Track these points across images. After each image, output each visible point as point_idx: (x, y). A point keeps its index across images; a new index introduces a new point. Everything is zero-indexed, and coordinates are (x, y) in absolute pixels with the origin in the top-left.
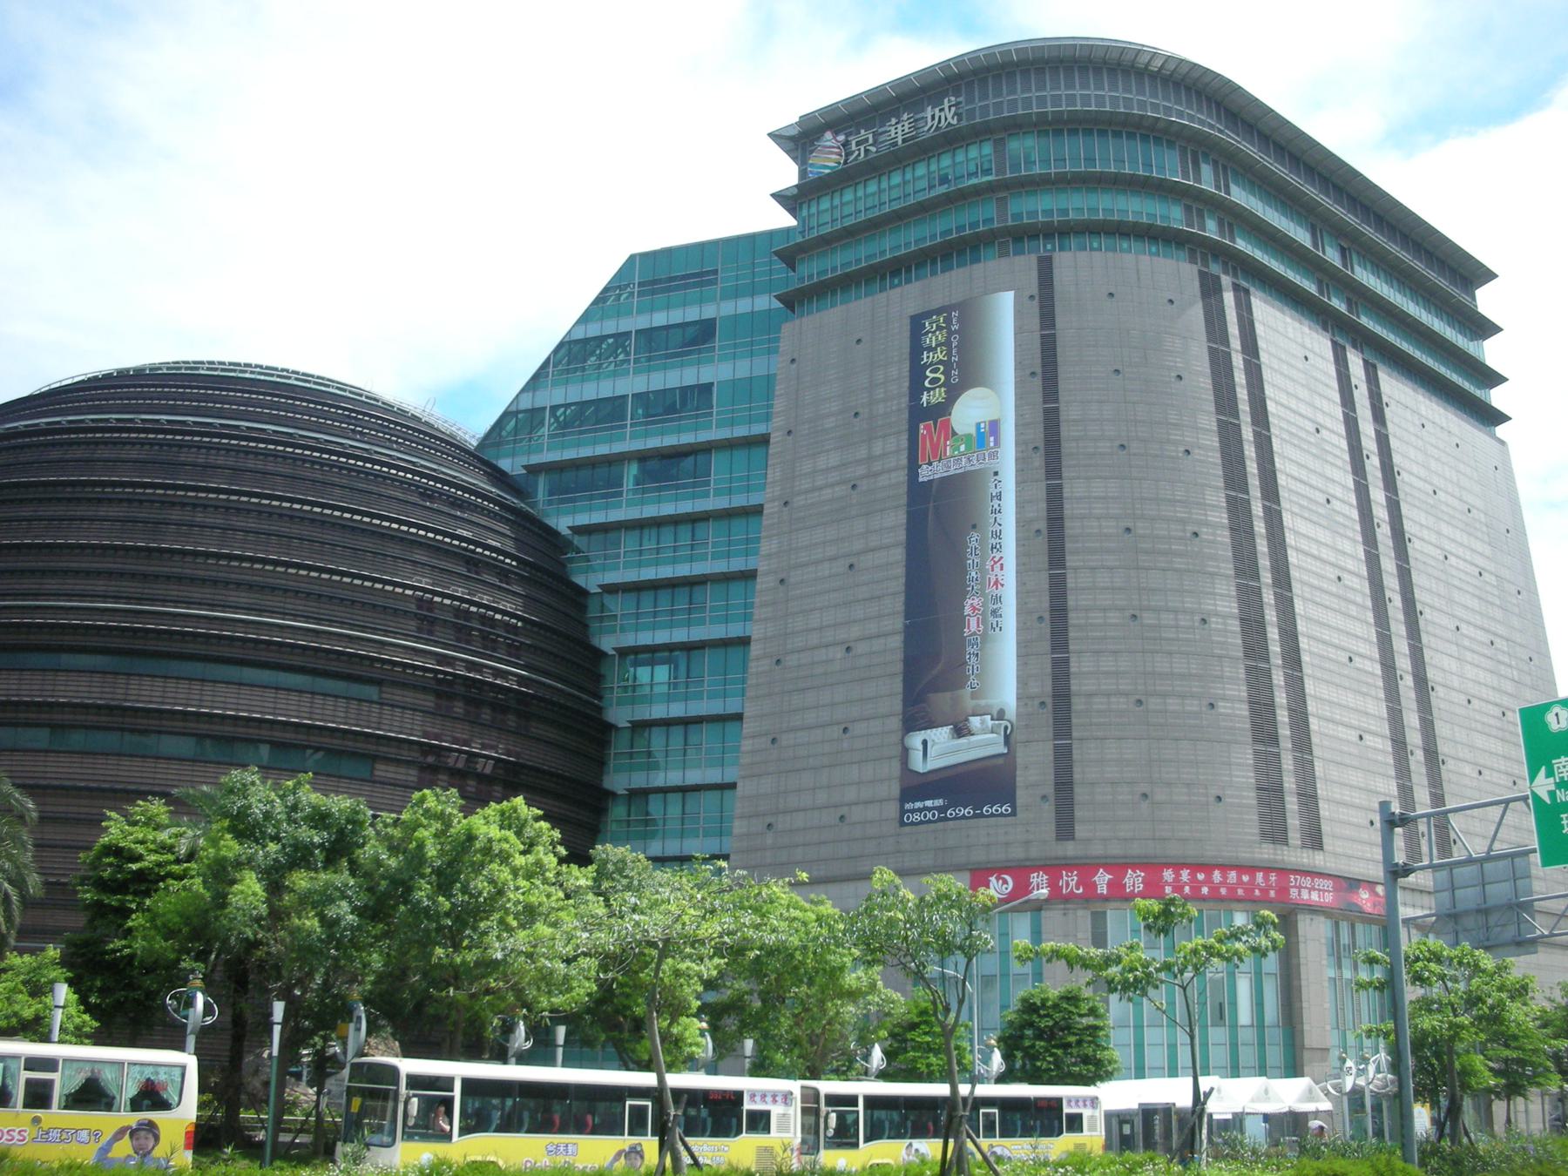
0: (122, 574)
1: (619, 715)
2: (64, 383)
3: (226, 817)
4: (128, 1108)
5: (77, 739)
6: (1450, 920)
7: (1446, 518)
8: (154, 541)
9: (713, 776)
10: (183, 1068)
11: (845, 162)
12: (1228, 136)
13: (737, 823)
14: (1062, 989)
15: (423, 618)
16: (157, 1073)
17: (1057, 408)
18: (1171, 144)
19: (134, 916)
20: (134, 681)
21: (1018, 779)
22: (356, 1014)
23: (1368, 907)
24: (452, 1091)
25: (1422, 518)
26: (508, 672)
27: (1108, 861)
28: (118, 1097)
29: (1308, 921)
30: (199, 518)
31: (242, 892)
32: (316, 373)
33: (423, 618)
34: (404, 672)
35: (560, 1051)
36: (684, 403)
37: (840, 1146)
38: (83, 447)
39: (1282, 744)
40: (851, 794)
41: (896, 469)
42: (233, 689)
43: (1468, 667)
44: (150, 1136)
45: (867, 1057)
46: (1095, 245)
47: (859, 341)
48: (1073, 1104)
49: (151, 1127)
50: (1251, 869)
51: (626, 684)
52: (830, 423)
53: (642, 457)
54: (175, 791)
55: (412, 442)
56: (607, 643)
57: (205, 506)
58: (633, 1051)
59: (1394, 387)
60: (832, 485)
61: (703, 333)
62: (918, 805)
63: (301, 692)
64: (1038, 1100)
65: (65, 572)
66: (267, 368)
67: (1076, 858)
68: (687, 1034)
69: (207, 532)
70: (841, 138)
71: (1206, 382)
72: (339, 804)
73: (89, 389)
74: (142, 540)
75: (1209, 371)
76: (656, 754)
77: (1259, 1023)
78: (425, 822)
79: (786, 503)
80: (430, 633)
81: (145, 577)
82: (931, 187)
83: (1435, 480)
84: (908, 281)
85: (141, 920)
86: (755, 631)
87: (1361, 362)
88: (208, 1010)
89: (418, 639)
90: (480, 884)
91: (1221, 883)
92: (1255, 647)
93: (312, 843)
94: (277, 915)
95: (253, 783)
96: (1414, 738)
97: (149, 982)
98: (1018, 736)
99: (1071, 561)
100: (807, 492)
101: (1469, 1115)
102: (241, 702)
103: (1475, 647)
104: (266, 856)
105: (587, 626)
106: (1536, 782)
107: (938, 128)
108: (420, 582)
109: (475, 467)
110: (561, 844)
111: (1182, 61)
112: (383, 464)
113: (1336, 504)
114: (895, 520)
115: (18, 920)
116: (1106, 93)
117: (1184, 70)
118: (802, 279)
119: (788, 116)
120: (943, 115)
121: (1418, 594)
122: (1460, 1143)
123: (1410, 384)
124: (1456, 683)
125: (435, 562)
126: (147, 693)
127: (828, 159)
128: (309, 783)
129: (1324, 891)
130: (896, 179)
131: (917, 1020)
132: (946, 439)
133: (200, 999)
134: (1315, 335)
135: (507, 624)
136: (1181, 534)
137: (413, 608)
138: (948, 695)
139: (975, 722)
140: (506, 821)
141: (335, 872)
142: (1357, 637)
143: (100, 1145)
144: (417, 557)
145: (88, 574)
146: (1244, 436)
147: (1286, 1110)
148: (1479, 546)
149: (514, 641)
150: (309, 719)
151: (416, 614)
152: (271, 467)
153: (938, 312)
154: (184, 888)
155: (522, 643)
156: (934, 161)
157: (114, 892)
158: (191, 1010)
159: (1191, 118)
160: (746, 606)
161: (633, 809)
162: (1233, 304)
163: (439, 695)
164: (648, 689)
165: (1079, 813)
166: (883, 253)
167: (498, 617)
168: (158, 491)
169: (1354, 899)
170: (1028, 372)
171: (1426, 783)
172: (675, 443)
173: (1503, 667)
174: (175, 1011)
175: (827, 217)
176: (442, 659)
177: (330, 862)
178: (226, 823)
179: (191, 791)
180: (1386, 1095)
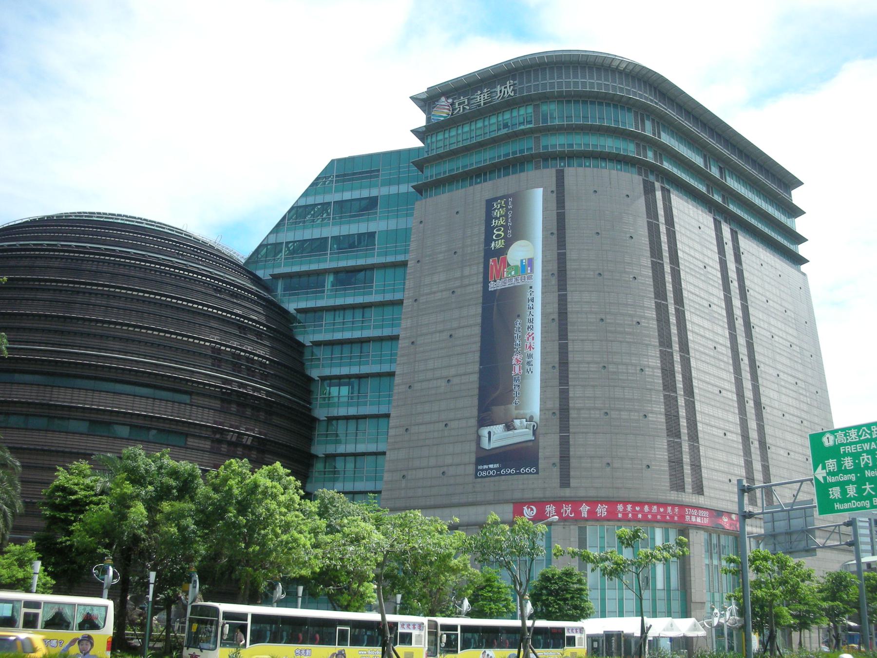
0: (49, 331)
1: (321, 413)
4: (77, 628)
6: (771, 537)
7: (774, 316)
8: (68, 312)
9: (372, 448)
10: (106, 607)
11: (452, 115)
12: (660, 106)
14: (563, 569)
15: (215, 358)
16: (92, 610)
17: (565, 253)
18: (629, 110)
20: (55, 390)
22: (193, 579)
23: (727, 526)
25: (760, 315)
26: (261, 389)
28: (72, 623)
29: (695, 533)
30: (93, 300)
32: (157, 220)
33: (215, 358)
34: (204, 388)
35: (300, 600)
36: (359, 242)
37: (448, 652)
40: (449, 460)
41: (477, 283)
43: (783, 396)
44: (89, 643)
46: (587, 164)
47: (457, 213)
48: (570, 631)
49: (89, 639)
50: (665, 505)
52: (441, 257)
53: (336, 271)
55: (210, 260)
56: (315, 374)
57: (96, 294)
59: (746, 244)
60: (442, 291)
61: (371, 203)
62: (485, 467)
63: (148, 398)
64: (552, 629)
67: (571, 497)
68: (367, 591)
69: (97, 308)
70: (450, 101)
71: (645, 240)
72: (184, 466)
73: (28, 227)
75: (647, 234)
76: (340, 435)
77: (668, 589)
78: (233, 477)
80: (219, 366)
81: (62, 332)
82: (499, 129)
83: (768, 294)
84: (485, 181)
85: (79, 527)
86: (398, 370)
90: (261, 510)
91: (648, 512)
92: (669, 384)
93: (171, 486)
94: (153, 525)
95: (140, 454)
96: (754, 435)
99: (570, 336)
100: (427, 294)
101: (779, 640)
103: (787, 385)
104: (147, 493)
105: (303, 364)
106: (816, 472)
107: (503, 98)
110: (301, 489)
111: (636, 65)
112: (194, 272)
113: (714, 307)
117: (637, 70)
119: (421, 88)
120: (506, 90)
122: (775, 655)
124: (776, 404)
125: (221, 327)
126: (63, 397)
127: (442, 112)
128: (168, 453)
129: (704, 517)
130: (480, 124)
132: (504, 268)
135: (261, 362)
137: (209, 353)
139: (517, 422)
140: (271, 476)
142: (724, 379)
143: (62, 648)
145: (31, 330)
146: (665, 270)
147: (682, 635)
148: (791, 331)
149: (264, 371)
150: (152, 413)
155: (268, 373)
157: (61, 511)
158: (106, 576)
160: (391, 355)
161: (327, 464)
163: (223, 400)
164: (336, 400)
167: (256, 358)
169: (720, 522)
170: (549, 233)
173: (801, 397)
175: (441, 144)
176: (225, 381)
177: (180, 498)
180: (735, 628)
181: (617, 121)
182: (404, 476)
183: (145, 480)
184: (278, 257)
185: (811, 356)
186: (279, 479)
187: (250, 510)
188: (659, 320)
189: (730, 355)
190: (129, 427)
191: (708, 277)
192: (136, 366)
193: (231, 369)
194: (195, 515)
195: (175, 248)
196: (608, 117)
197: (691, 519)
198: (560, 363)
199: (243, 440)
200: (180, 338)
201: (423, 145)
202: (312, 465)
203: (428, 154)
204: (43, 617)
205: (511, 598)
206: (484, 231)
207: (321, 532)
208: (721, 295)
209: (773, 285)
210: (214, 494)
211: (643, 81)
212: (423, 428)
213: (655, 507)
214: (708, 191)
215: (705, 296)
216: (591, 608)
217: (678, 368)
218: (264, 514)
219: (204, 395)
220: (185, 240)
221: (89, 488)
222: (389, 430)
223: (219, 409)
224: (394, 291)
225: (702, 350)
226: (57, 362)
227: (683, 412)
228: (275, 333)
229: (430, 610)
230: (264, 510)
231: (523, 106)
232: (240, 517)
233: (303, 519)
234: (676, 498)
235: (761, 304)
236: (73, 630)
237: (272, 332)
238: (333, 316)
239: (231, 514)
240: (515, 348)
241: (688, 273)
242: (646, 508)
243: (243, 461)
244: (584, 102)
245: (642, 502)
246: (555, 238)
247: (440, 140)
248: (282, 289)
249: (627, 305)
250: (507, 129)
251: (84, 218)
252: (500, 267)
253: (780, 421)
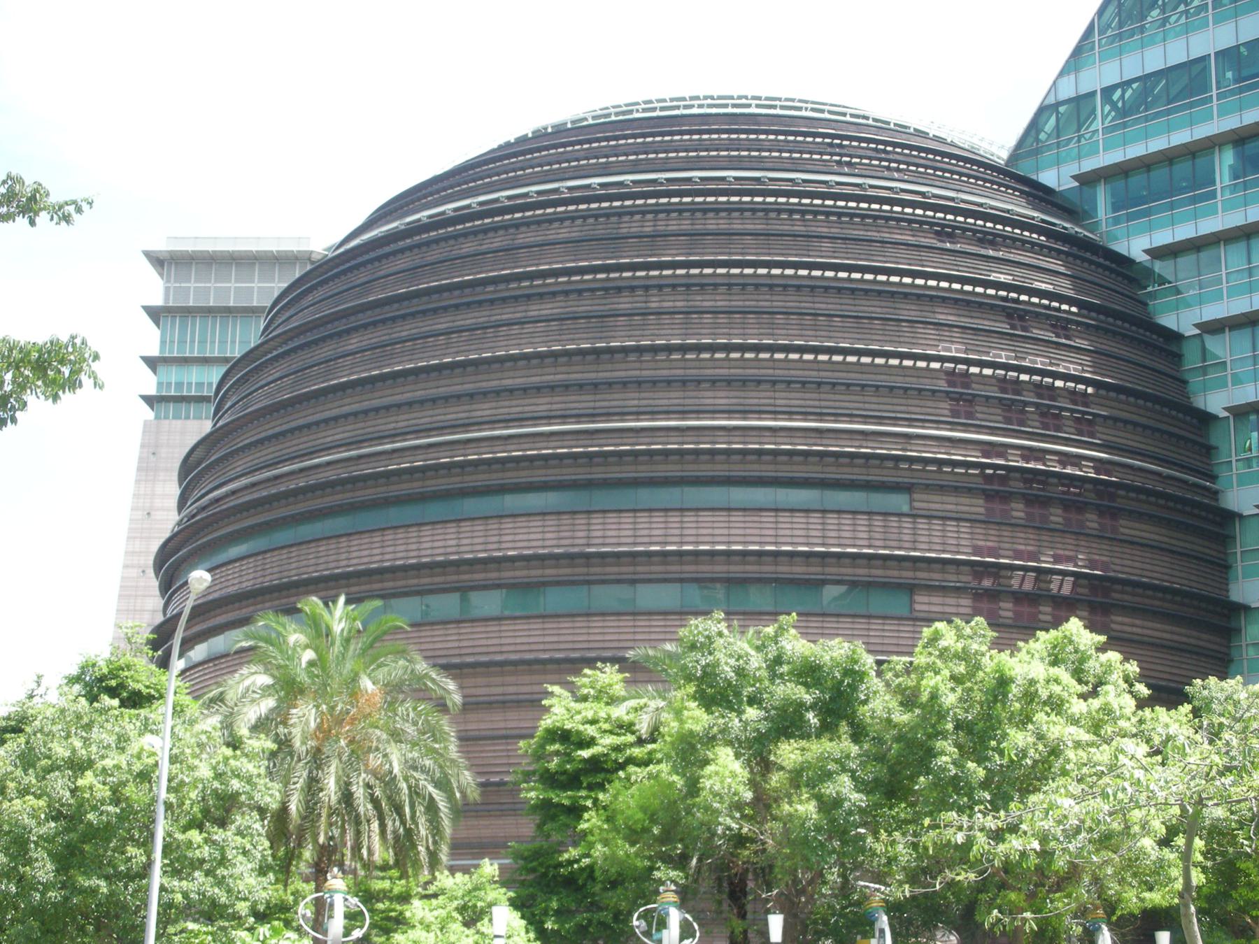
0: (566, 387)
3: (691, 680)
5: (554, 599)
8: (601, 339)
15: (957, 398)
19: (586, 816)
20: (597, 520)
22: (877, 926)
31: (717, 773)
33: (957, 398)
38: (501, 232)
42: (721, 517)
51: (1248, 455)
54: (630, 654)
56: (1216, 402)
57: (660, 287)
63: (807, 511)
65: (498, 393)
66: (720, 98)
69: (666, 319)
73: (500, 159)
80: (970, 415)
81: (596, 386)
89: (953, 426)
94: (762, 804)
95: (720, 634)
97: (615, 899)
102: (733, 532)
105: (1185, 382)
108: (949, 350)
109: (1007, 187)
115: (448, 831)
125: (965, 321)
128: (794, 627)
135: (1073, 392)
137: (942, 385)
141: (831, 740)
144: (941, 318)
149: (1084, 413)
151: (947, 393)
157: (564, 787)
158: (665, 932)
163: (989, 496)
167: (1059, 383)
168: (625, 274)
174: (644, 933)
177: (827, 729)
178: (691, 689)
179: (651, 652)
183: (738, 694)
187: (993, 743)
193: (1000, 418)
195: (829, 150)
199: (1052, 586)
202: (1238, 631)
219: (942, 489)
220: (853, 128)
223: (982, 518)
226: (590, 456)
228: (1102, 317)
237: (1093, 315)
239: (944, 758)
243: (973, 623)
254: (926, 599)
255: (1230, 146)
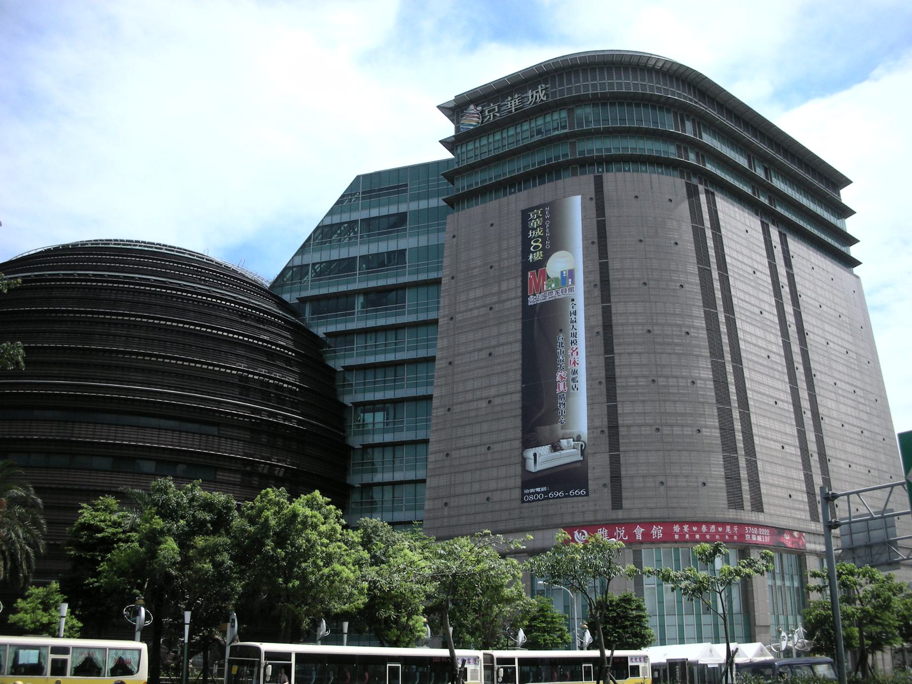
1: (356, 442)
2: (31, 253)
4: (109, 674)
7: (828, 321)
8: (87, 344)
9: (411, 476)
10: (140, 651)
11: (482, 122)
13: (426, 503)
17: (607, 262)
18: (668, 111)
19: (102, 564)
21: (589, 475)
23: (789, 545)
24: (291, 661)
25: (814, 321)
26: (292, 418)
27: (642, 521)
28: (103, 668)
35: (345, 636)
39: (739, 452)
40: (493, 485)
43: (842, 406)
45: (516, 635)
46: (627, 169)
47: (492, 225)
48: (634, 660)
50: (723, 524)
52: (476, 272)
53: (366, 292)
56: (348, 400)
58: (387, 636)
59: (796, 247)
60: (478, 308)
61: (398, 222)
62: (532, 490)
66: (149, 243)
68: (417, 625)
70: (479, 108)
71: (691, 246)
72: (219, 497)
73: (39, 257)
74: (80, 344)
78: (269, 507)
79: (452, 319)
82: (532, 136)
83: (820, 299)
84: (520, 190)
85: (106, 567)
86: (436, 392)
87: (777, 233)
88: (147, 617)
90: (301, 541)
91: (706, 532)
94: (186, 562)
96: (813, 447)
98: (589, 450)
99: (617, 349)
102: (125, 435)
103: (845, 394)
111: (673, 63)
113: (765, 314)
114: (515, 327)
116: (631, 81)
117: (675, 68)
118: (458, 190)
119: (448, 96)
120: (538, 95)
121: (813, 365)
122: (868, 677)
123: (805, 244)
124: (835, 414)
125: (248, 354)
126: (84, 433)
127: (472, 120)
129: (765, 535)
130: (512, 132)
131: (537, 614)
132: (544, 280)
133: (143, 610)
134: (751, 217)
135: (290, 390)
136: (679, 333)
138: (548, 427)
139: (564, 442)
140: (310, 505)
142: (779, 390)
146: (714, 277)
147: (749, 661)
150: (179, 446)
151: (239, 386)
152: (153, 301)
153: (537, 208)
154: (129, 547)
156: (533, 121)
159: (679, 96)
161: (364, 495)
162: (705, 201)
164: (371, 427)
165: (624, 494)
166: (504, 174)
167: (285, 385)
170: (590, 241)
171: (820, 473)
172: (385, 284)
173: (861, 405)
175: (471, 154)
176: (254, 411)
177: (215, 532)
178: (154, 510)
181: (655, 123)
182: (446, 504)
183: (176, 514)
184: (305, 279)
185: (869, 362)
186: (319, 508)
187: (289, 542)
188: (708, 330)
189: (785, 364)
190: (155, 462)
191: (758, 283)
192: (160, 397)
194: (231, 548)
195: (196, 273)
196: (646, 119)
197: (751, 538)
198: (607, 378)
200: (206, 367)
201: (453, 157)
203: (459, 165)
204: (73, 662)
205: (565, 628)
206: (521, 243)
207: (365, 563)
208: (773, 301)
209: (825, 290)
210: (250, 527)
211: (688, 83)
212: (464, 452)
213: (713, 527)
214: (754, 193)
215: (756, 302)
216: (652, 636)
217: (731, 379)
218: (304, 545)
220: (207, 265)
221: (116, 524)
222: (429, 456)
224: (427, 310)
225: (755, 359)
227: (738, 425)
229: (484, 643)
230: (304, 541)
231: (549, 113)
232: (279, 550)
233: (346, 550)
234: (735, 517)
235: (813, 309)
236: (104, 676)
238: (384, 336)
240: (559, 365)
241: (737, 279)
242: (704, 528)
244: (621, 104)
245: (699, 522)
246: (596, 247)
247: (470, 150)
248: (310, 312)
249: (674, 314)
250: (541, 135)
251: (101, 246)
252: (539, 280)
253: (839, 431)
254: (221, 474)
255: (362, 295)
